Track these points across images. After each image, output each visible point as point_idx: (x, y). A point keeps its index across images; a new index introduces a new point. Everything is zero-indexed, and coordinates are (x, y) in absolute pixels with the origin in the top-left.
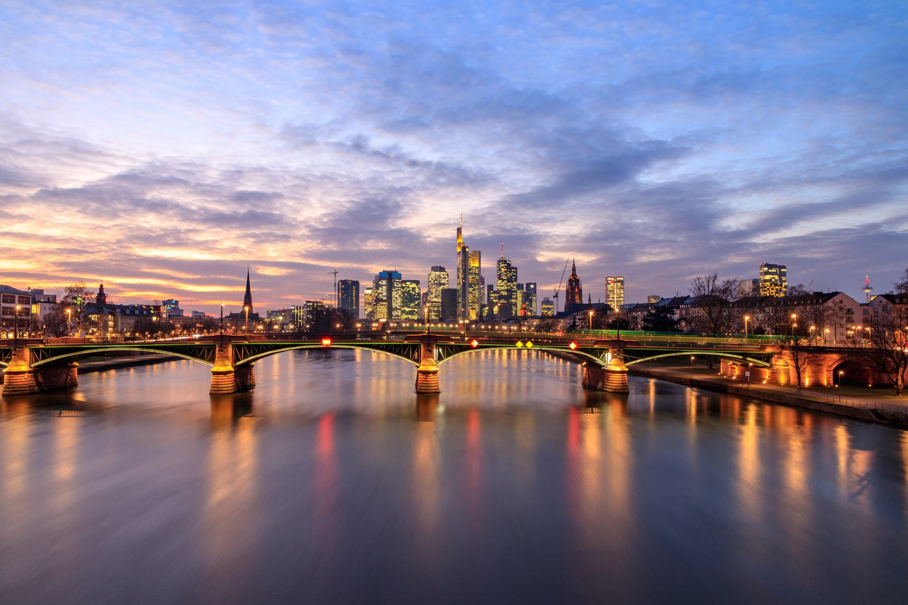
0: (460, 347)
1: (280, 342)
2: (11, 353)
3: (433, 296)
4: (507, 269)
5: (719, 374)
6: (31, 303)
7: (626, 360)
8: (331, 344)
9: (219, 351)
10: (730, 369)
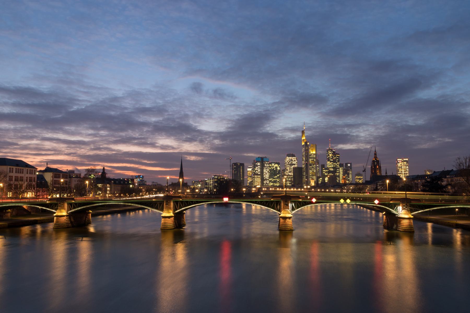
2: (58, 205)
3: (288, 172)
4: (333, 155)
7: (411, 211)
9: (166, 204)
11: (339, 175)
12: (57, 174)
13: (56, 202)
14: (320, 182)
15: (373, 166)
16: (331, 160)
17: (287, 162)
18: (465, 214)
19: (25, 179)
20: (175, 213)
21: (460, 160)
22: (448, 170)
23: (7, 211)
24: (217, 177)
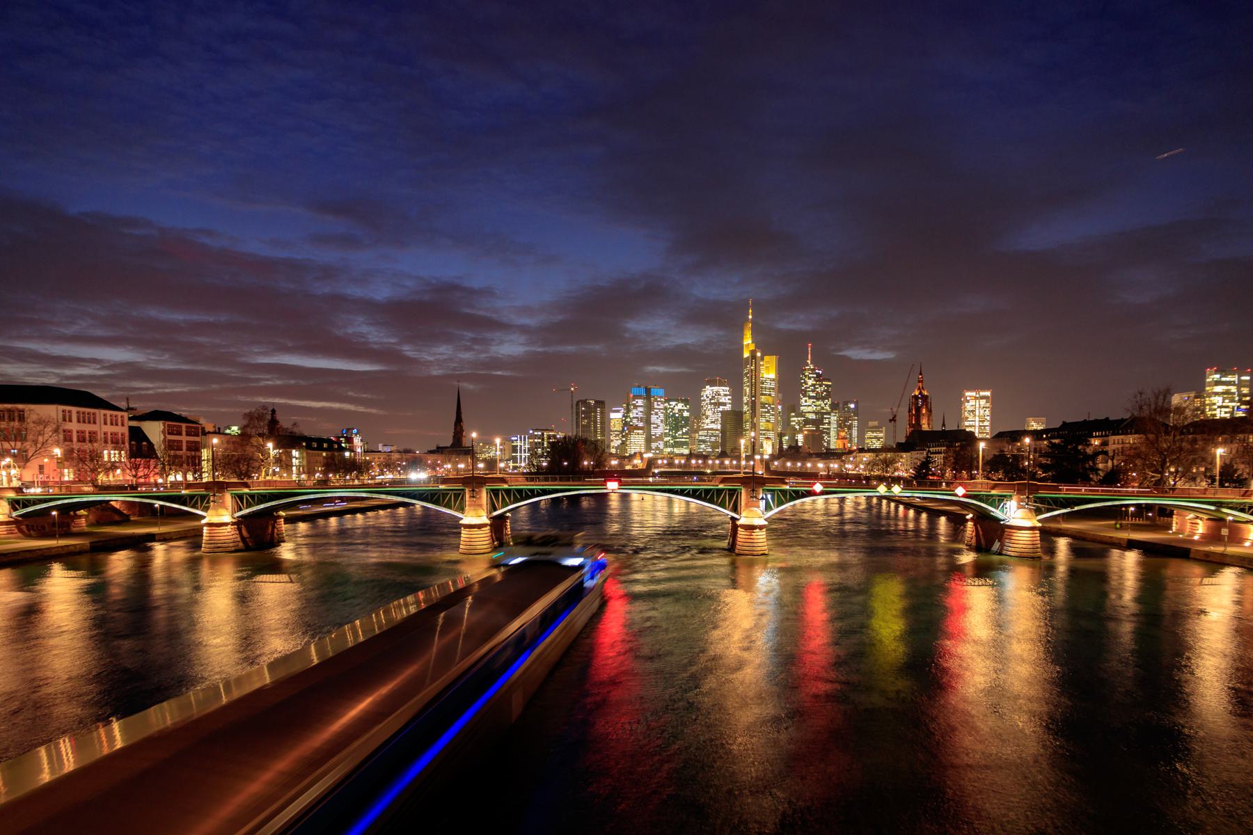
0: (796, 492)
1: (550, 485)
2: (209, 499)
3: (708, 421)
4: (817, 381)
5: (1171, 532)
6: (200, 434)
7: (1038, 511)
8: (619, 489)
9: (471, 497)
10: (1189, 524)
11: (829, 429)
12: (174, 426)
13: (204, 493)
14: (785, 447)
15: (913, 408)
16: (811, 394)
17: (708, 397)
18: (1143, 520)
19: (100, 436)
20: (491, 518)
21: (1144, 396)
22: (1096, 420)
23: (78, 512)
24: (540, 433)
